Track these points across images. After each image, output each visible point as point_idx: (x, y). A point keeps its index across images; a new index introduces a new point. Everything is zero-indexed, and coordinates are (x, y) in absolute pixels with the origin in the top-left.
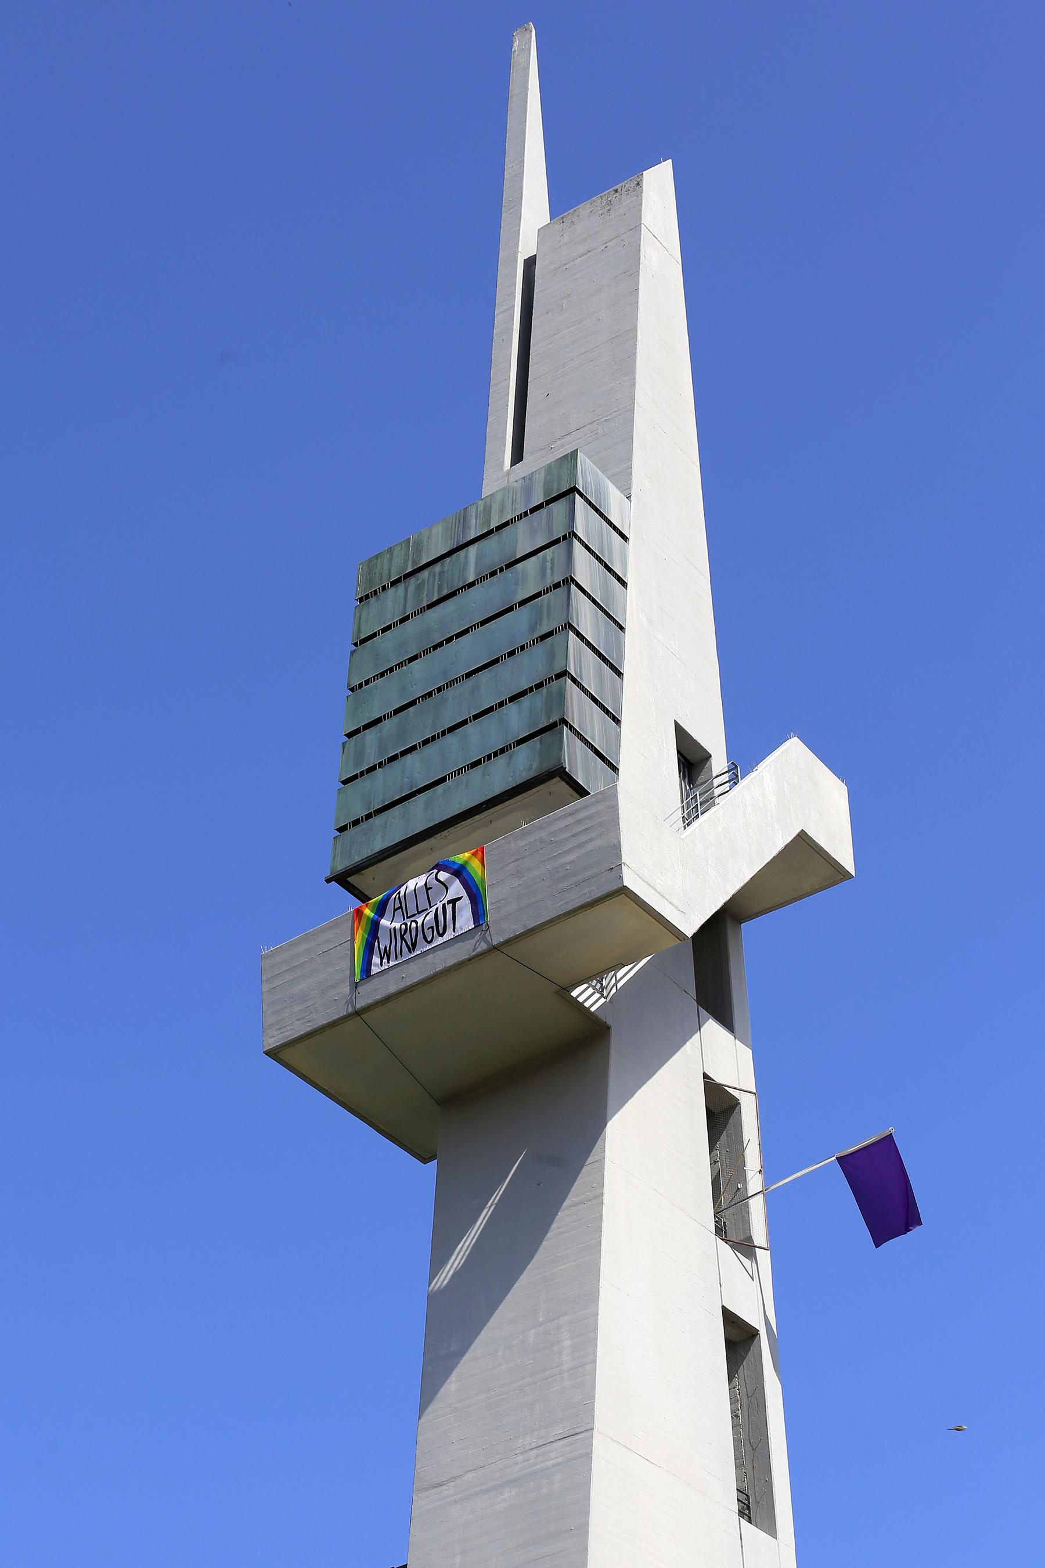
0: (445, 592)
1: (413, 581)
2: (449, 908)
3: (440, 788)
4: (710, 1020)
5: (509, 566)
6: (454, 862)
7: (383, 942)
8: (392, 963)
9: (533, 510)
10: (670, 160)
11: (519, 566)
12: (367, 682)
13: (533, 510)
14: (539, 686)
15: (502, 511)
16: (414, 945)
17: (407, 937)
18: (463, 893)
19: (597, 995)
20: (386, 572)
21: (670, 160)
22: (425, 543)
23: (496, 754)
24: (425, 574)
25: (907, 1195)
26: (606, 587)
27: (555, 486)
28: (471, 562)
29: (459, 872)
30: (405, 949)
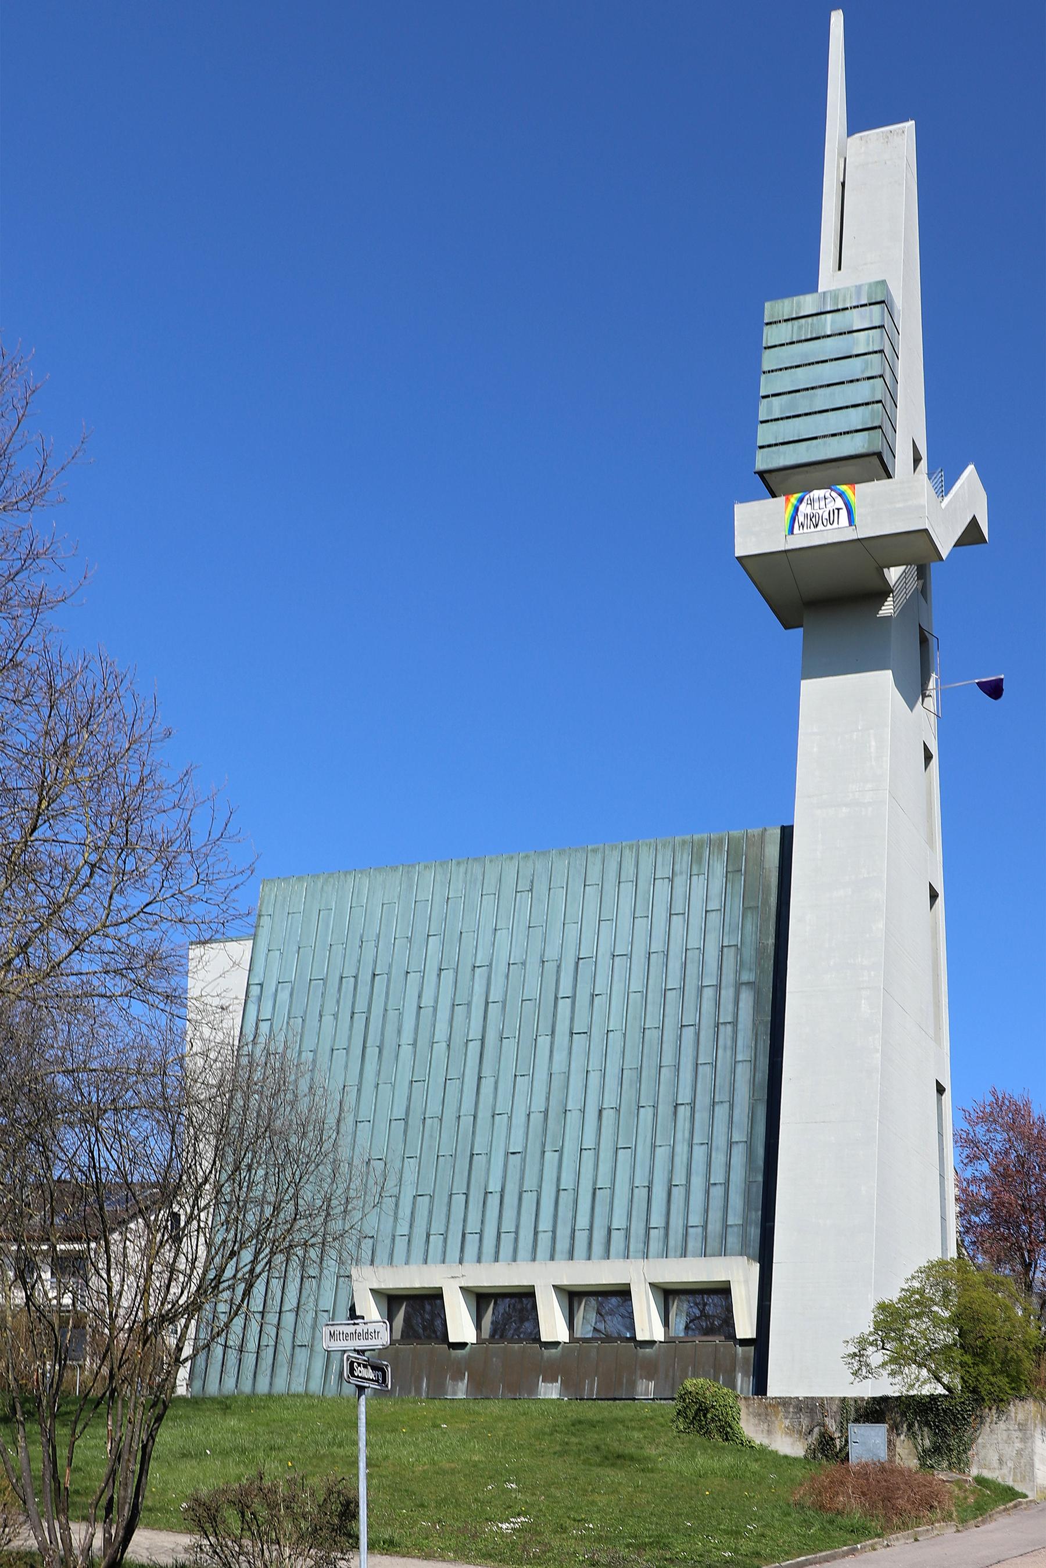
0: (814, 336)
1: (796, 322)
2: (836, 511)
3: (814, 442)
4: (886, 677)
5: (849, 332)
6: (839, 489)
7: (801, 518)
8: (809, 530)
9: (862, 306)
10: (911, 123)
11: (855, 334)
12: (772, 371)
13: (862, 306)
14: (867, 404)
15: (844, 301)
16: (817, 525)
17: (813, 520)
18: (843, 506)
19: (892, 607)
20: (781, 313)
21: (911, 123)
22: (802, 303)
23: (844, 433)
24: (803, 321)
25: (379, 1292)
26: (893, 358)
27: (874, 296)
28: (828, 324)
29: (841, 495)
30: (812, 526)
